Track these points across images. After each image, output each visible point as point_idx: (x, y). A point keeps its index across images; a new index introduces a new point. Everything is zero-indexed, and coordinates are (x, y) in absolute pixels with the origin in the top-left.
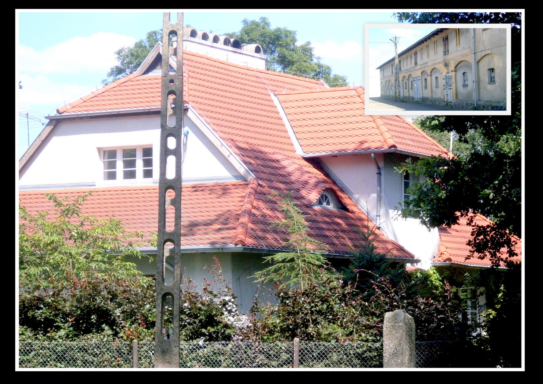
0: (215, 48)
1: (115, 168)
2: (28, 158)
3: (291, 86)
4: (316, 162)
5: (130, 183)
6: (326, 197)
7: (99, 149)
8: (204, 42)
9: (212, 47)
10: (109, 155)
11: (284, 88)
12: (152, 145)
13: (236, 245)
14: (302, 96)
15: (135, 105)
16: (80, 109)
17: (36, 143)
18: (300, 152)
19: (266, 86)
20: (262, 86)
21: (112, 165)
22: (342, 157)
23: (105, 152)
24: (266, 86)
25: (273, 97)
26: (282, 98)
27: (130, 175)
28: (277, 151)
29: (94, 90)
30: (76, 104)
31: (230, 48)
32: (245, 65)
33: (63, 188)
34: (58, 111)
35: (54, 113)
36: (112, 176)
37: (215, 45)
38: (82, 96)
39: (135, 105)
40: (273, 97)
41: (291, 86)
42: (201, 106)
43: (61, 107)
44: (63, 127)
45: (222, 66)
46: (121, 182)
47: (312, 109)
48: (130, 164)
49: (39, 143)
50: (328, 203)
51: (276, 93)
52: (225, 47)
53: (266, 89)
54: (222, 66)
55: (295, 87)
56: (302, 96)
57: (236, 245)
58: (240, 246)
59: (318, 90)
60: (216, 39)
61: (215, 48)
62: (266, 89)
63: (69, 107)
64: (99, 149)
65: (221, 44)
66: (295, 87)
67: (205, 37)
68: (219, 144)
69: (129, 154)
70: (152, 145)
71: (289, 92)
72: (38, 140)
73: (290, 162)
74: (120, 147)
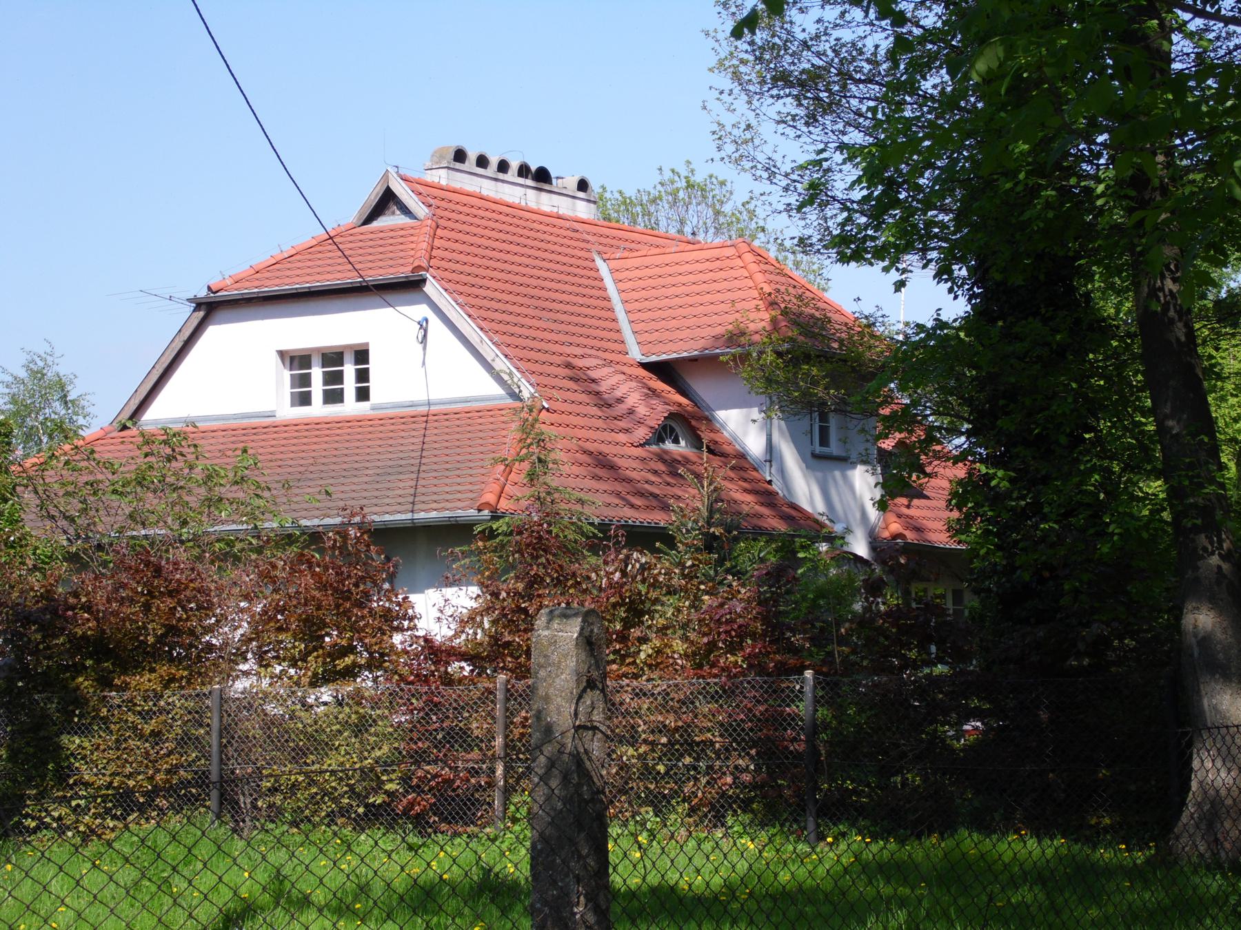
0: (503, 181)
1: (309, 385)
2: (161, 371)
3: (628, 245)
4: (664, 370)
5: (334, 410)
6: (672, 430)
7: (282, 354)
8: (480, 171)
9: (496, 180)
10: (298, 361)
11: (618, 248)
12: (367, 344)
13: (480, 510)
14: (647, 261)
15: (339, 275)
16: (248, 284)
17: (173, 345)
18: (636, 353)
19: (588, 246)
20: (583, 245)
21: (305, 380)
22: (704, 362)
23: (292, 359)
24: (588, 246)
25: (599, 263)
26: (614, 264)
27: (333, 397)
28: (593, 352)
29: (276, 252)
30: (242, 276)
31: (530, 182)
32: (555, 210)
33: (222, 422)
34: (209, 288)
35: (203, 294)
36: (305, 399)
37: (501, 176)
38: (253, 263)
39: (339, 275)
40: (599, 263)
41: (628, 245)
42: (447, 275)
43: (215, 282)
44: (221, 314)
45: (535, 217)
46: (318, 409)
47: (661, 281)
48: (334, 378)
49: (178, 345)
50: (676, 441)
51: (606, 256)
52: (521, 180)
53: (589, 251)
54: (535, 217)
55: (633, 246)
56: (647, 261)
57: (480, 510)
58: (486, 512)
59: (673, 250)
60: (503, 166)
61: (503, 181)
62: (589, 251)
63: (229, 282)
64: (282, 354)
65: (512, 175)
66: (633, 246)
67: (482, 161)
68: (478, 340)
69: (333, 358)
70: (367, 344)
71: (626, 254)
72: (177, 340)
73: (606, 370)
74: (317, 350)
